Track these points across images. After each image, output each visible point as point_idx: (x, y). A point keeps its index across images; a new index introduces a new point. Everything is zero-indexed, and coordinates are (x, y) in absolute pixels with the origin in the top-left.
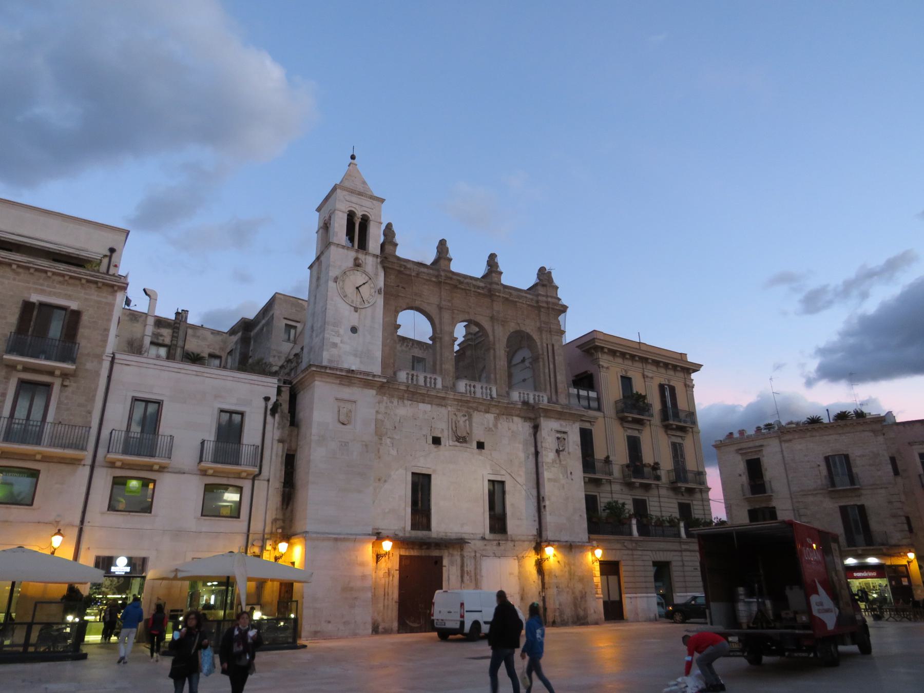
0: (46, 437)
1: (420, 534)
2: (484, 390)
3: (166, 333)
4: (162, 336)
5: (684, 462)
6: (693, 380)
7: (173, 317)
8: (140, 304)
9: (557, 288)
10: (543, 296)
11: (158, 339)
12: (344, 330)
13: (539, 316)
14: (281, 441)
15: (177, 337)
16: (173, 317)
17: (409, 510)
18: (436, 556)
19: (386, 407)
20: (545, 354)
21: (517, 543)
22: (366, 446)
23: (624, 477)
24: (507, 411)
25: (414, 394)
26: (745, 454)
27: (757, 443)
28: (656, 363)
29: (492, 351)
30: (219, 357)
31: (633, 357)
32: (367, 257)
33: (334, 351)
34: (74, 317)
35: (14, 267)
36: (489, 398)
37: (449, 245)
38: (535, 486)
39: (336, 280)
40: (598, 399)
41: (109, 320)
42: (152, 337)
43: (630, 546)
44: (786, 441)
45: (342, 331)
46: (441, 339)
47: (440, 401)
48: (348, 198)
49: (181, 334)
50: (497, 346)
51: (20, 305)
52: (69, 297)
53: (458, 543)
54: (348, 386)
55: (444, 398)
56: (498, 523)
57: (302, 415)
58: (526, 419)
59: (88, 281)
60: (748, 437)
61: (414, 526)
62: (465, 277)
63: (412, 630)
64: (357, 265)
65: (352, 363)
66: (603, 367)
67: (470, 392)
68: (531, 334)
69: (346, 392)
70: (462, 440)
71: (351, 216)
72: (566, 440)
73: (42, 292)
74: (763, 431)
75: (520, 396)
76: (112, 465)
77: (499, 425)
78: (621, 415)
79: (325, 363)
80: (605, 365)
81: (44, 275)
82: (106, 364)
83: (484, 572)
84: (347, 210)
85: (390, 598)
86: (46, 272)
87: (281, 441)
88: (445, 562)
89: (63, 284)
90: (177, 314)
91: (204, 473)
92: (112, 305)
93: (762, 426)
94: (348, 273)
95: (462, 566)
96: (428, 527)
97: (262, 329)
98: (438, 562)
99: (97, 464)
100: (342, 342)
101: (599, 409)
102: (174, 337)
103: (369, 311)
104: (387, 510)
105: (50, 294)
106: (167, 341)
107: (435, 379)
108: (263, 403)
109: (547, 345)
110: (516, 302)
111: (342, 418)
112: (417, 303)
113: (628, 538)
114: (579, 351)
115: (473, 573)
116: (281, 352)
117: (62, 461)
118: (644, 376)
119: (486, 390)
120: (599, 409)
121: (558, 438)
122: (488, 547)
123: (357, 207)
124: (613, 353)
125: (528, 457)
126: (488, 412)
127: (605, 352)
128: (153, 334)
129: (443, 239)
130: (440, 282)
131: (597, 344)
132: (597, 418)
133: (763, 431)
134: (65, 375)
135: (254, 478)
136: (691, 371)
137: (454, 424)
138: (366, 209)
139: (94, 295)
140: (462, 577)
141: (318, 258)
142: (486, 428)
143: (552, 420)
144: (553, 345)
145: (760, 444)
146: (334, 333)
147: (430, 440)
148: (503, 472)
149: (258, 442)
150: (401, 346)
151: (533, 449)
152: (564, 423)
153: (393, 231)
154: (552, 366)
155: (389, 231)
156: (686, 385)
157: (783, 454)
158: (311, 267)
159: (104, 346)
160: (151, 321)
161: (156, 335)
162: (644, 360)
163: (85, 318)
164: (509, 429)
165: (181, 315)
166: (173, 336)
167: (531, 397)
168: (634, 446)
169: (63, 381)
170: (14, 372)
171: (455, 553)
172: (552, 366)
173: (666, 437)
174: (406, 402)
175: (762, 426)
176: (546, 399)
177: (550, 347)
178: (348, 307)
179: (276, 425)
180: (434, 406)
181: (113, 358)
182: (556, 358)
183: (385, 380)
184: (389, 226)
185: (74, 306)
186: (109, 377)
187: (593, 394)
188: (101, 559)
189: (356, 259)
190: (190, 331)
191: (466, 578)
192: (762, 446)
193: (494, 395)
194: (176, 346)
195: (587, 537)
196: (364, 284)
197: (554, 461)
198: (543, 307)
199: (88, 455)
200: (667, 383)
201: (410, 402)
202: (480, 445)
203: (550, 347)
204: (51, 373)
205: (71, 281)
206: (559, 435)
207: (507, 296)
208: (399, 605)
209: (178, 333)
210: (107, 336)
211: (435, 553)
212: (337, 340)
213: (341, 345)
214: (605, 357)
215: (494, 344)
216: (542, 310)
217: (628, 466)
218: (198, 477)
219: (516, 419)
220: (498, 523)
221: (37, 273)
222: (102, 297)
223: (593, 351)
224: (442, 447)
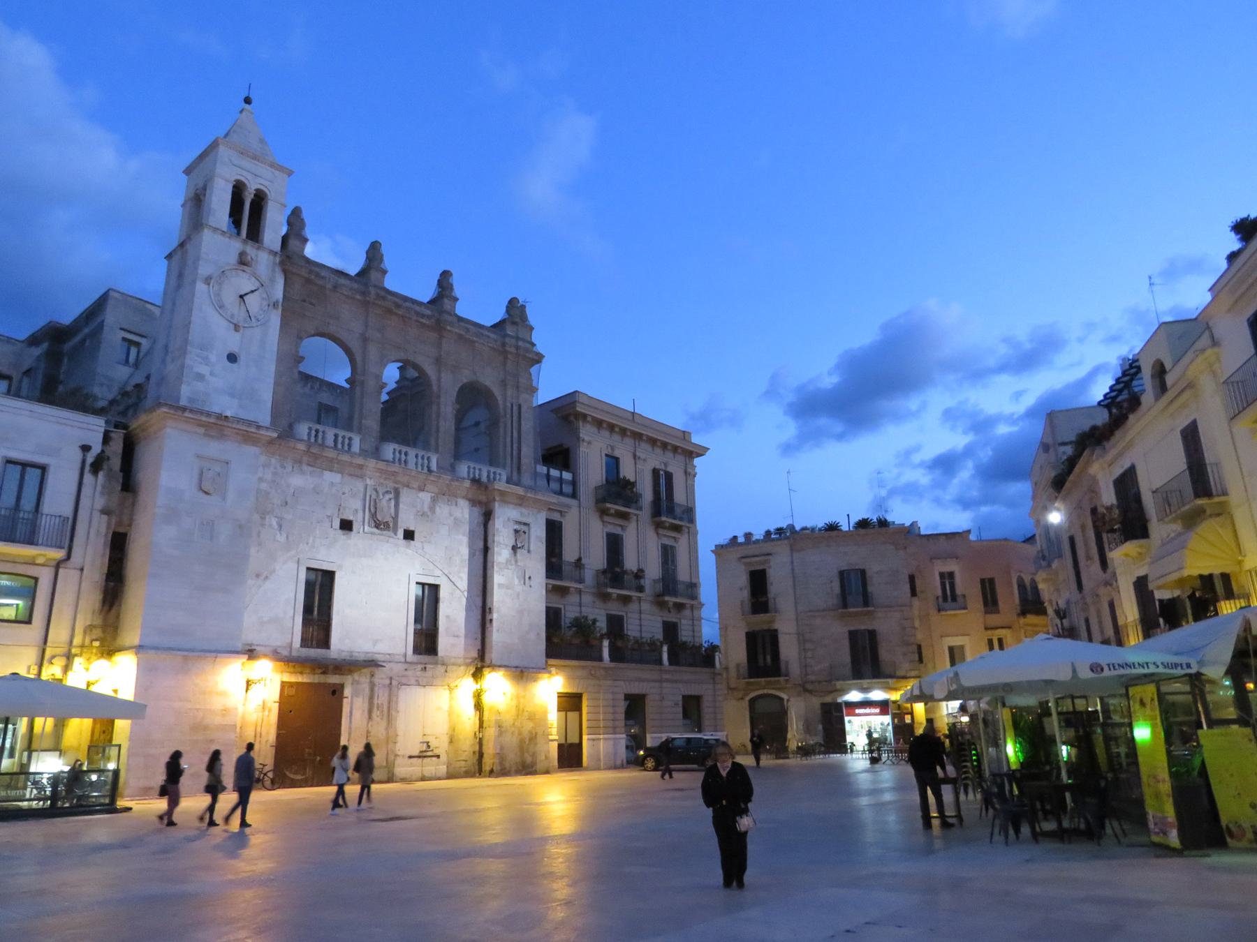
6: (696, 467)
9: (532, 329)
12: (217, 356)
13: (504, 364)
14: (105, 511)
18: (335, 684)
20: (508, 416)
28: (653, 442)
33: (200, 386)
37: (384, 250)
39: (207, 280)
40: (574, 483)
45: (213, 358)
63: (294, 784)
69: (214, 448)
72: (527, 534)
75: (469, 472)
77: (438, 510)
84: (233, 179)
87: (105, 511)
94: (227, 273)
95: (371, 698)
100: (212, 374)
101: (574, 495)
108: (78, 455)
110: (474, 342)
112: (332, 329)
120: (574, 495)
122: (410, 673)
123: (249, 176)
129: (376, 242)
133: (773, 536)
138: (262, 181)
142: (419, 512)
144: (520, 407)
146: (200, 360)
147: (337, 524)
153: (302, 220)
154: (515, 434)
158: (169, 257)
164: (451, 515)
168: (614, 545)
177: (515, 408)
179: (99, 488)
182: (523, 423)
187: (567, 476)
191: (376, 713)
198: (511, 353)
203: (515, 408)
206: (517, 527)
208: (276, 753)
211: (334, 679)
212: (204, 370)
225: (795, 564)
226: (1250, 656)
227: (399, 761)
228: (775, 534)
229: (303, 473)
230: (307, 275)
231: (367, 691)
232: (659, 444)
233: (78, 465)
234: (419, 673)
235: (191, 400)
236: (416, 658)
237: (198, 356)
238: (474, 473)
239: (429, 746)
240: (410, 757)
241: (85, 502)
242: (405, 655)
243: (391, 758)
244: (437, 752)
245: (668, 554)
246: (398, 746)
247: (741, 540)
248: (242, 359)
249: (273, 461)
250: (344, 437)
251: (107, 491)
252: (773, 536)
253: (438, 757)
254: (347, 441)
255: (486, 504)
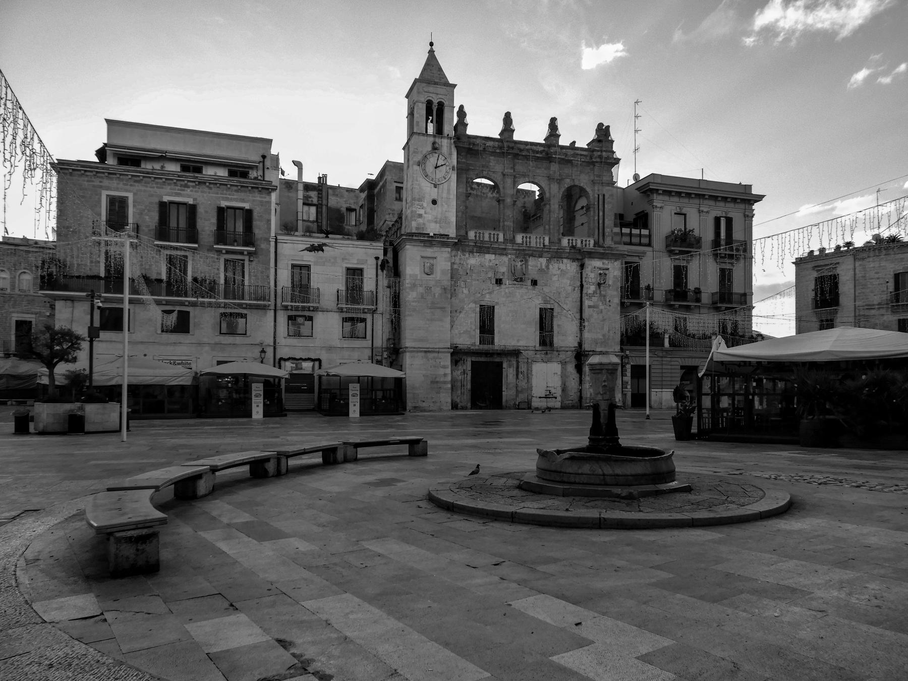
0: (247, 296)
1: (486, 347)
2: (538, 240)
3: (313, 194)
4: (310, 197)
5: (731, 286)
7: (316, 181)
8: (291, 174)
9: (612, 142)
10: (598, 151)
11: (308, 200)
12: (427, 203)
14: (389, 287)
15: (321, 198)
16: (316, 181)
17: (478, 331)
18: (498, 362)
19: (460, 259)
21: (560, 353)
22: (445, 289)
23: (667, 300)
24: (557, 255)
25: (481, 248)
26: (819, 270)
27: (834, 261)
28: (715, 198)
29: (548, 206)
30: (355, 210)
31: (688, 195)
32: (443, 140)
33: (420, 220)
34: (248, 215)
35: (207, 184)
36: (542, 246)
37: (513, 116)
38: (579, 311)
40: (650, 236)
41: (270, 213)
42: (303, 199)
43: (661, 354)
44: (860, 260)
45: (425, 205)
46: (504, 200)
47: (502, 252)
48: (426, 89)
49: (324, 194)
50: (552, 202)
51: (216, 210)
52: (243, 201)
53: (515, 353)
54: (430, 247)
55: (505, 249)
56: (546, 340)
57: (401, 268)
58: (574, 260)
59: (252, 188)
60: (827, 255)
61: (482, 342)
62: (526, 143)
63: (481, 408)
64: (435, 148)
65: (432, 229)
66: (656, 207)
67: (526, 242)
68: (585, 187)
69: (429, 252)
70: (519, 280)
71: (429, 104)
73: (227, 199)
74: (842, 249)
75: (569, 243)
76: (286, 308)
77: (551, 266)
78: (669, 248)
79: (414, 231)
80: (659, 205)
81: (225, 187)
82: (273, 244)
83: (534, 373)
85: (465, 388)
86: (226, 185)
87: (389, 287)
88: (505, 365)
89: (238, 192)
90: (319, 178)
91: (341, 310)
92: (269, 202)
93: (842, 245)
94: (428, 156)
95: (518, 368)
96: (493, 343)
97: (380, 189)
98: (500, 365)
99: (277, 308)
100: (425, 213)
101: (649, 245)
102: (320, 198)
103: (446, 185)
104: (462, 332)
105: (231, 200)
106: (315, 201)
107: (498, 235)
108: (375, 261)
109: (599, 195)
111: (427, 270)
113: (660, 348)
114: (638, 192)
115: (525, 372)
116: (394, 210)
117: (258, 307)
118: (700, 212)
119: (540, 239)
120: (649, 245)
121: (600, 274)
122: (538, 356)
123: (434, 96)
124: (668, 193)
125: (574, 290)
126: (542, 257)
127: (660, 194)
128: (304, 196)
129: (508, 112)
130: (503, 153)
131: (651, 187)
132: (644, 253)
133: (842, 249)
134: (250, 254)
135: (374, 312)
136: (752, 202)
137: (513, 268)
138: (440, 96)
139: (257, 197)
140: (517, 375)
141: (407, 143)
143: (596, 259)
144: (604, 195)
145: (837, 261)
146: (419, 207)
147: (494, 281)
148: (552, 302)
149: (373, 288)
150: (492, 194)
151: (579, 284)
152: (606, 262)
153: (465, 112)
154: (601, 214)
155: (462, 113)
156: (746, 216)
157: (855, 271)
158: (404, 149)
159: (270, 233)
160: (301, 187)
161: (306, 198)
162: (700, 196)
163: (255, 215)
164: (559, 269)
165: (322, 179)
166: (319, 197)
167: (579, 242)
168: (680, 274)
169: (250, 258)
170: (222, 255)
171: (512, 359)
172: (601, 214)
173: (715, 264)
174: (475, 254)
175: (842, 245)
176: (592, 242)
177: (601, 197)
178: (430, 184)
179: (385, 276)
180: (497, 255)
181: (276, 239)
182: (606, 206)
183: (457, 241)
184: (461, 107)
185: (247, 206)
186: (276, 252)
187: (645, 232)
188: (593, 437)
189: (434, 143)
190: (330, 191)
191: (520, 376)
192: (838, 263)
193: (547, 243)
194: (321, 205)
195: (619, 348)
196: (442, 165)
197: (595, 292)
198: (597, 162)
199: (272, 303)
200: (724, 215)
201: (478, 254)
202: (534, 283)
203: (601, 197)
204: (241, 253)
205: (243, 189)
207: (563, 157)
208: (472, 393)
209: (321, 194)
210: (270, 224)
211: (497, 360)
212: (422, 212)
213: (425, 215)
214: (660, 197)
215: (550, 200)
216: (596, 164)
217: (670, 291)
218: (338, 314)
219: (565, 261)
220: (546, 340)
221: (222, 187)
222: (264, 198)
223: (649, 193)
224: (503, 286)
225: (857, 270)
226: (129, 386)
227: (534, 399)
228: (844, 247)
229: (474, 257)
230: (467, 146)
231: (515, 365)
232: (720, 199)
233: (375, 266)
234: (543, 356)
235: (417, 228)
236: (540, 348)
237: (418, 205)
238: (572, 243)
239: (550, 393)
240: (540, 398)
241: (380, 283)
242: (535, 347)
243: (530, 398)
244: (555, 395)
245: (725, 277)
246: (533, 392)
247: (816, 253)
248: (439, 203)
249: (459, 252)
250: (494, 234)
251: (388, 276)
252: (842, 249)
253: (556, 398)
254: (496, 236)
255: (581, 259)
